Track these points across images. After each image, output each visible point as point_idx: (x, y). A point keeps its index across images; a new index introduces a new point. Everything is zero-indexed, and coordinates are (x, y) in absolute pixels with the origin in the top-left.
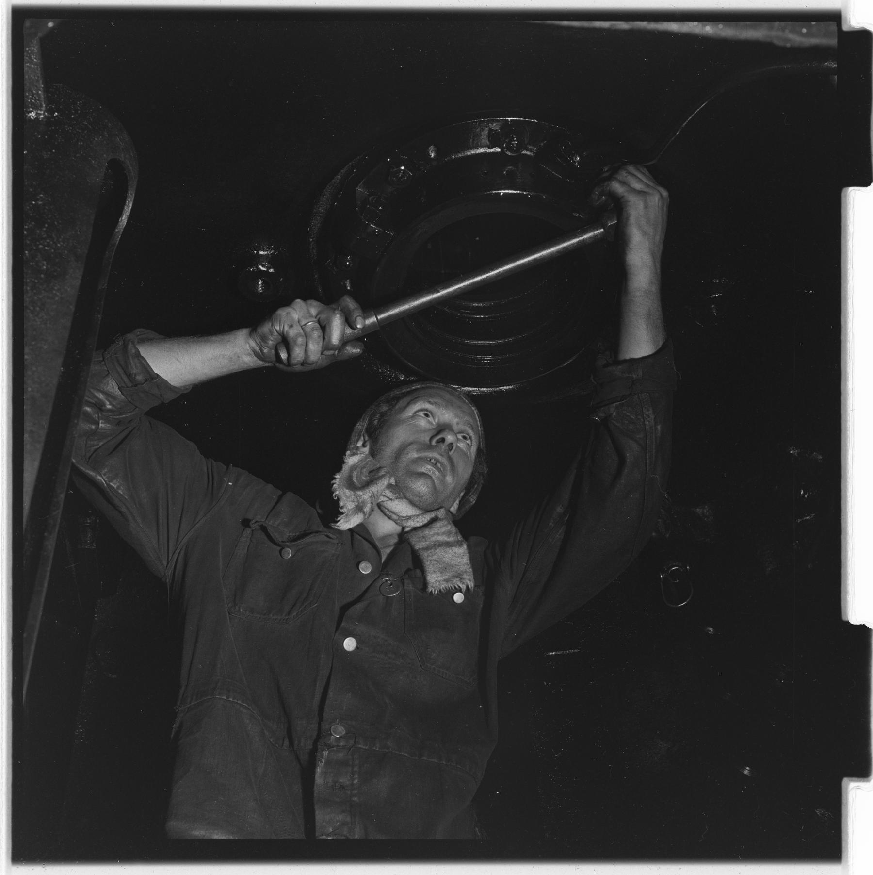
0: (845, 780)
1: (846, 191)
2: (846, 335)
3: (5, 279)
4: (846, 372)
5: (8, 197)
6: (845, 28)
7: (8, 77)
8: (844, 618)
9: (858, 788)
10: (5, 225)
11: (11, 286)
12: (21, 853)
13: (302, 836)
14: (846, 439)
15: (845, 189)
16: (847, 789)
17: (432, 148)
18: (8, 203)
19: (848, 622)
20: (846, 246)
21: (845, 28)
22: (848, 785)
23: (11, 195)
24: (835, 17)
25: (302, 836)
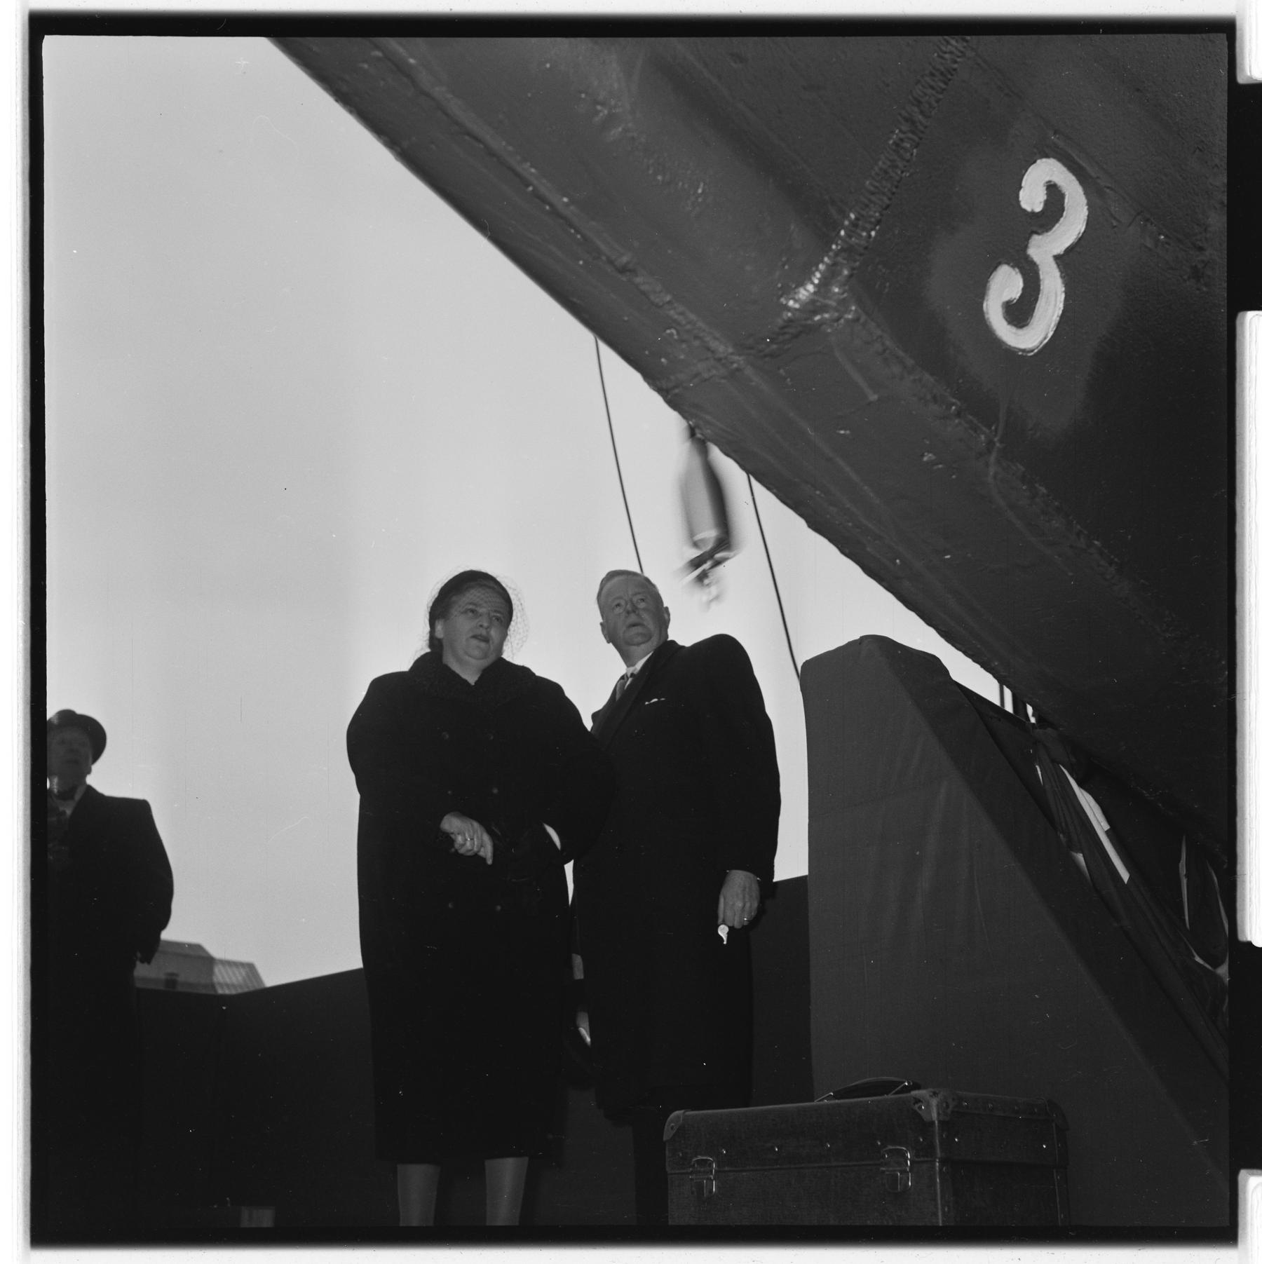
0: (1243, 1174)
1: (1244, 317)
2: (1243, 526)
6: (1241, 80)
7: (25, 791)
8: (1241, 938)
12: (47, 1227)
13: (399, 1167)
15: (1240, 314)
16: (1245, 1186)
17: (452, 824)
18: (25, 719)
19: (1250, 944)
20: (1243, 397)
21: (1241, 80)
22: (1246, 1181)
25: (399, 1167)
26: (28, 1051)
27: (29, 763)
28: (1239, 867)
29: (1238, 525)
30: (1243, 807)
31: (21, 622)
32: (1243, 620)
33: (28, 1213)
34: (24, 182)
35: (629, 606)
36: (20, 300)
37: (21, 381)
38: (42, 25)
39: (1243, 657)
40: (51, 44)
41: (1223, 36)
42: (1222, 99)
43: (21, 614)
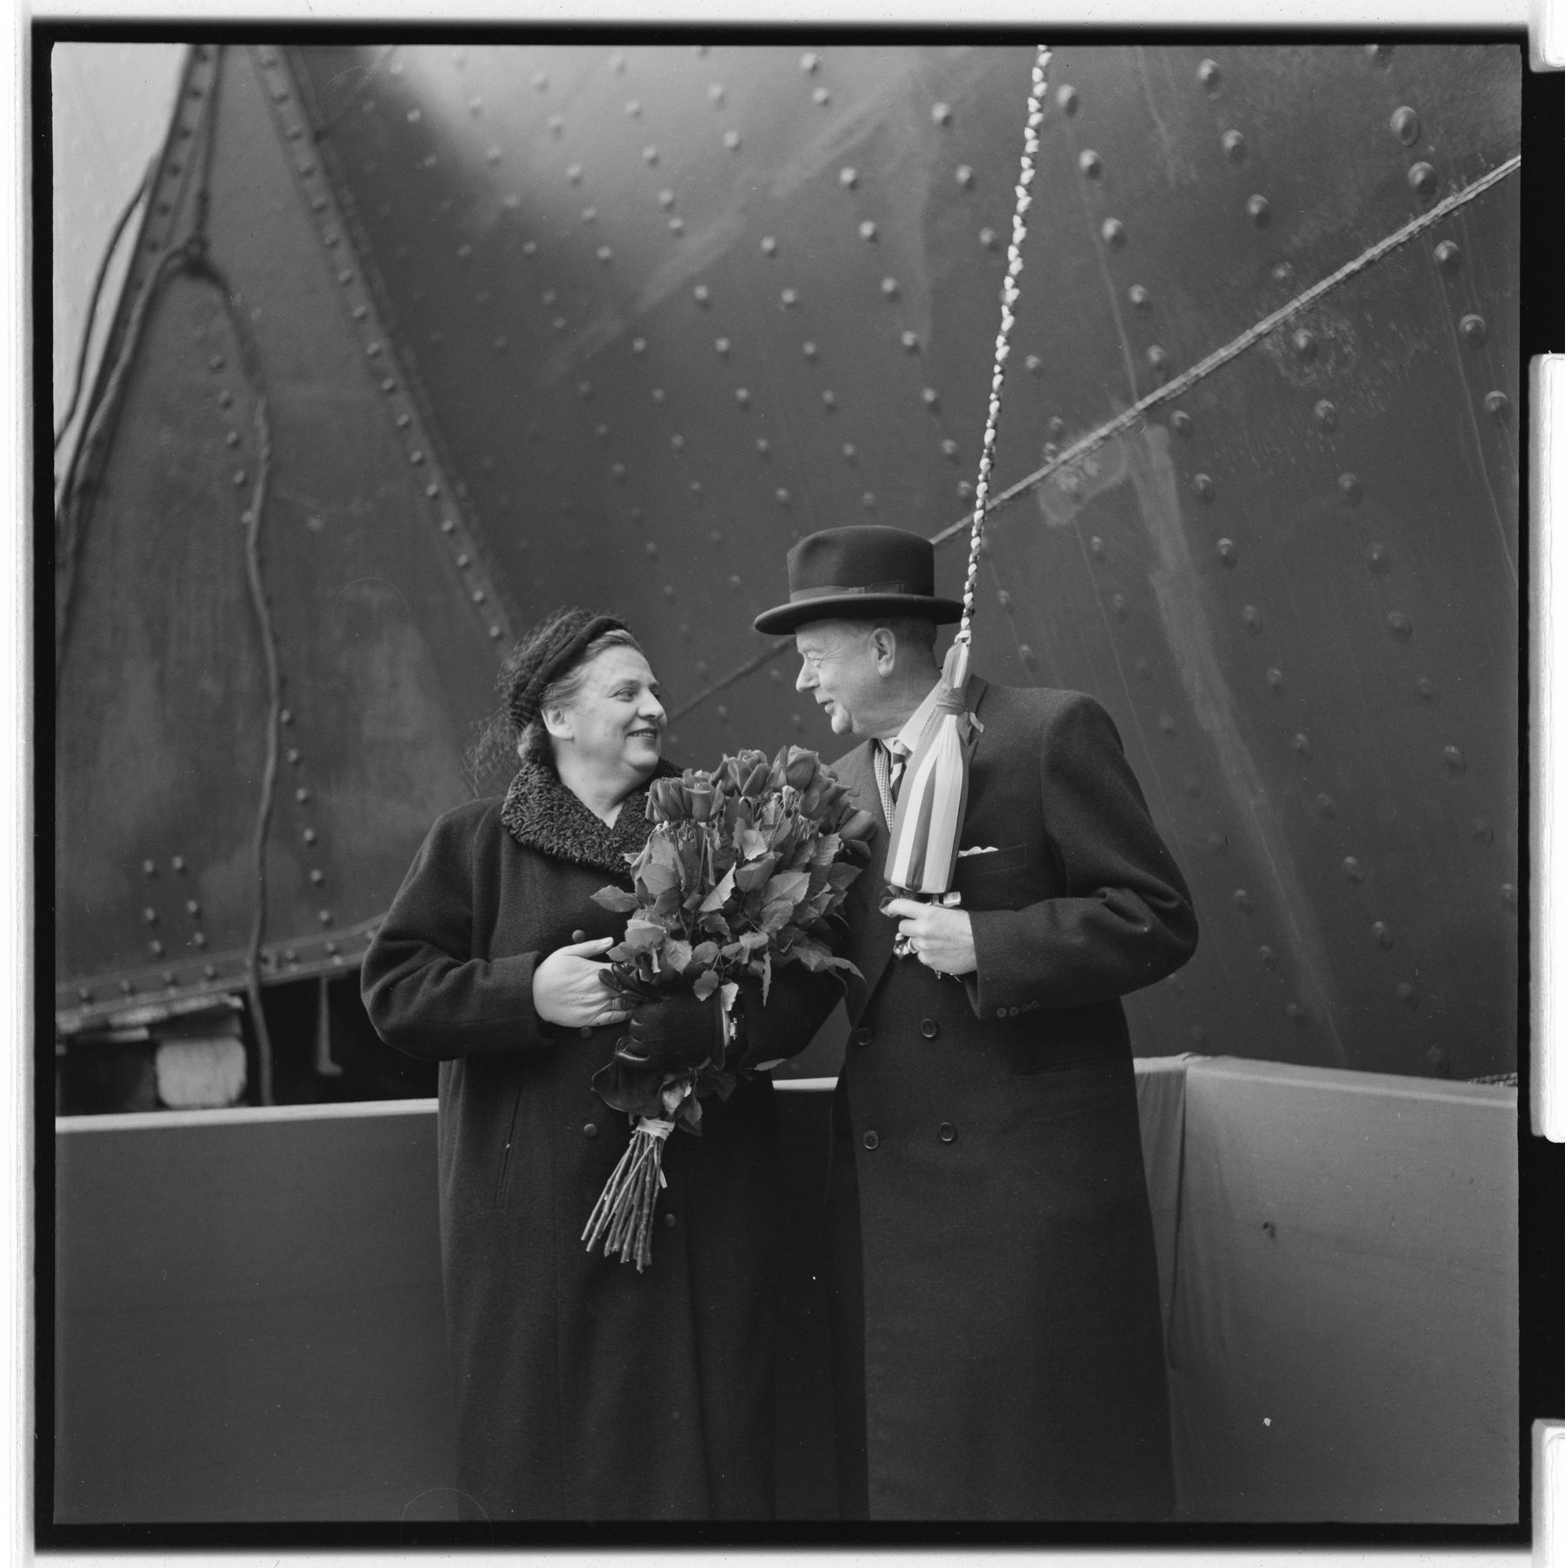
0: (1538, 1424)
3: (21, 522)
4: (1537, 686)
5: (26, 375)
6: (1535, 67)
7: (25, 159)
8: (1536, 1132)
9: (1562, 1437)
10: (21, 425)
11: (31, 611)
12: (50, 1532)
14: (1538, 807)
15: (1534, 359)
16: (1540, 1439)
19: (1544, 1139)
20: (1537, 461)
21: (1535, 67)
22: (1542, 1433)
23: (30, 302)
24: (1517, 38)
26: (32, 1273)
27: (33, 1329)
28: (1532, 1044)
29: (1532, 1015)
30: (1538, 970)
31: (22, 741)
32: (1537, 737)
33: (32, 1473)
34: (25, 195)
35: (776, 912)
36: (20, 340)
37: (21, 442)
38: (45, 35)
39: (1541, 1469)
40: (61, 53)
41: (1517, 48)
42: (1516, 86)
43: (21, 731)
